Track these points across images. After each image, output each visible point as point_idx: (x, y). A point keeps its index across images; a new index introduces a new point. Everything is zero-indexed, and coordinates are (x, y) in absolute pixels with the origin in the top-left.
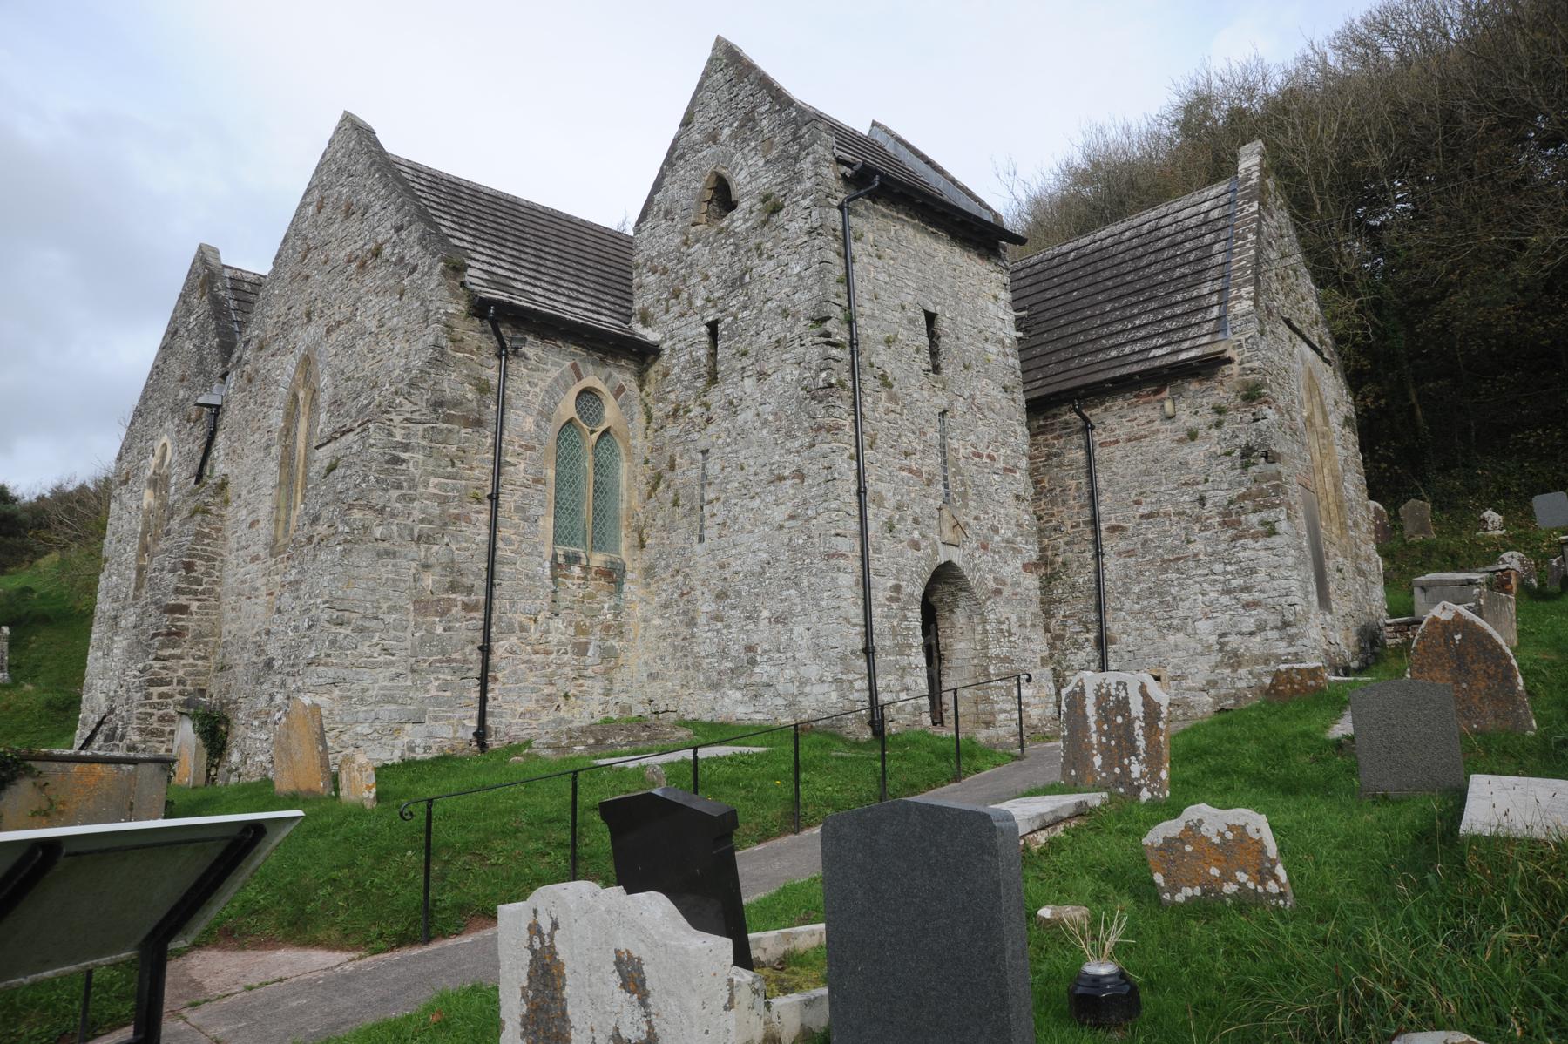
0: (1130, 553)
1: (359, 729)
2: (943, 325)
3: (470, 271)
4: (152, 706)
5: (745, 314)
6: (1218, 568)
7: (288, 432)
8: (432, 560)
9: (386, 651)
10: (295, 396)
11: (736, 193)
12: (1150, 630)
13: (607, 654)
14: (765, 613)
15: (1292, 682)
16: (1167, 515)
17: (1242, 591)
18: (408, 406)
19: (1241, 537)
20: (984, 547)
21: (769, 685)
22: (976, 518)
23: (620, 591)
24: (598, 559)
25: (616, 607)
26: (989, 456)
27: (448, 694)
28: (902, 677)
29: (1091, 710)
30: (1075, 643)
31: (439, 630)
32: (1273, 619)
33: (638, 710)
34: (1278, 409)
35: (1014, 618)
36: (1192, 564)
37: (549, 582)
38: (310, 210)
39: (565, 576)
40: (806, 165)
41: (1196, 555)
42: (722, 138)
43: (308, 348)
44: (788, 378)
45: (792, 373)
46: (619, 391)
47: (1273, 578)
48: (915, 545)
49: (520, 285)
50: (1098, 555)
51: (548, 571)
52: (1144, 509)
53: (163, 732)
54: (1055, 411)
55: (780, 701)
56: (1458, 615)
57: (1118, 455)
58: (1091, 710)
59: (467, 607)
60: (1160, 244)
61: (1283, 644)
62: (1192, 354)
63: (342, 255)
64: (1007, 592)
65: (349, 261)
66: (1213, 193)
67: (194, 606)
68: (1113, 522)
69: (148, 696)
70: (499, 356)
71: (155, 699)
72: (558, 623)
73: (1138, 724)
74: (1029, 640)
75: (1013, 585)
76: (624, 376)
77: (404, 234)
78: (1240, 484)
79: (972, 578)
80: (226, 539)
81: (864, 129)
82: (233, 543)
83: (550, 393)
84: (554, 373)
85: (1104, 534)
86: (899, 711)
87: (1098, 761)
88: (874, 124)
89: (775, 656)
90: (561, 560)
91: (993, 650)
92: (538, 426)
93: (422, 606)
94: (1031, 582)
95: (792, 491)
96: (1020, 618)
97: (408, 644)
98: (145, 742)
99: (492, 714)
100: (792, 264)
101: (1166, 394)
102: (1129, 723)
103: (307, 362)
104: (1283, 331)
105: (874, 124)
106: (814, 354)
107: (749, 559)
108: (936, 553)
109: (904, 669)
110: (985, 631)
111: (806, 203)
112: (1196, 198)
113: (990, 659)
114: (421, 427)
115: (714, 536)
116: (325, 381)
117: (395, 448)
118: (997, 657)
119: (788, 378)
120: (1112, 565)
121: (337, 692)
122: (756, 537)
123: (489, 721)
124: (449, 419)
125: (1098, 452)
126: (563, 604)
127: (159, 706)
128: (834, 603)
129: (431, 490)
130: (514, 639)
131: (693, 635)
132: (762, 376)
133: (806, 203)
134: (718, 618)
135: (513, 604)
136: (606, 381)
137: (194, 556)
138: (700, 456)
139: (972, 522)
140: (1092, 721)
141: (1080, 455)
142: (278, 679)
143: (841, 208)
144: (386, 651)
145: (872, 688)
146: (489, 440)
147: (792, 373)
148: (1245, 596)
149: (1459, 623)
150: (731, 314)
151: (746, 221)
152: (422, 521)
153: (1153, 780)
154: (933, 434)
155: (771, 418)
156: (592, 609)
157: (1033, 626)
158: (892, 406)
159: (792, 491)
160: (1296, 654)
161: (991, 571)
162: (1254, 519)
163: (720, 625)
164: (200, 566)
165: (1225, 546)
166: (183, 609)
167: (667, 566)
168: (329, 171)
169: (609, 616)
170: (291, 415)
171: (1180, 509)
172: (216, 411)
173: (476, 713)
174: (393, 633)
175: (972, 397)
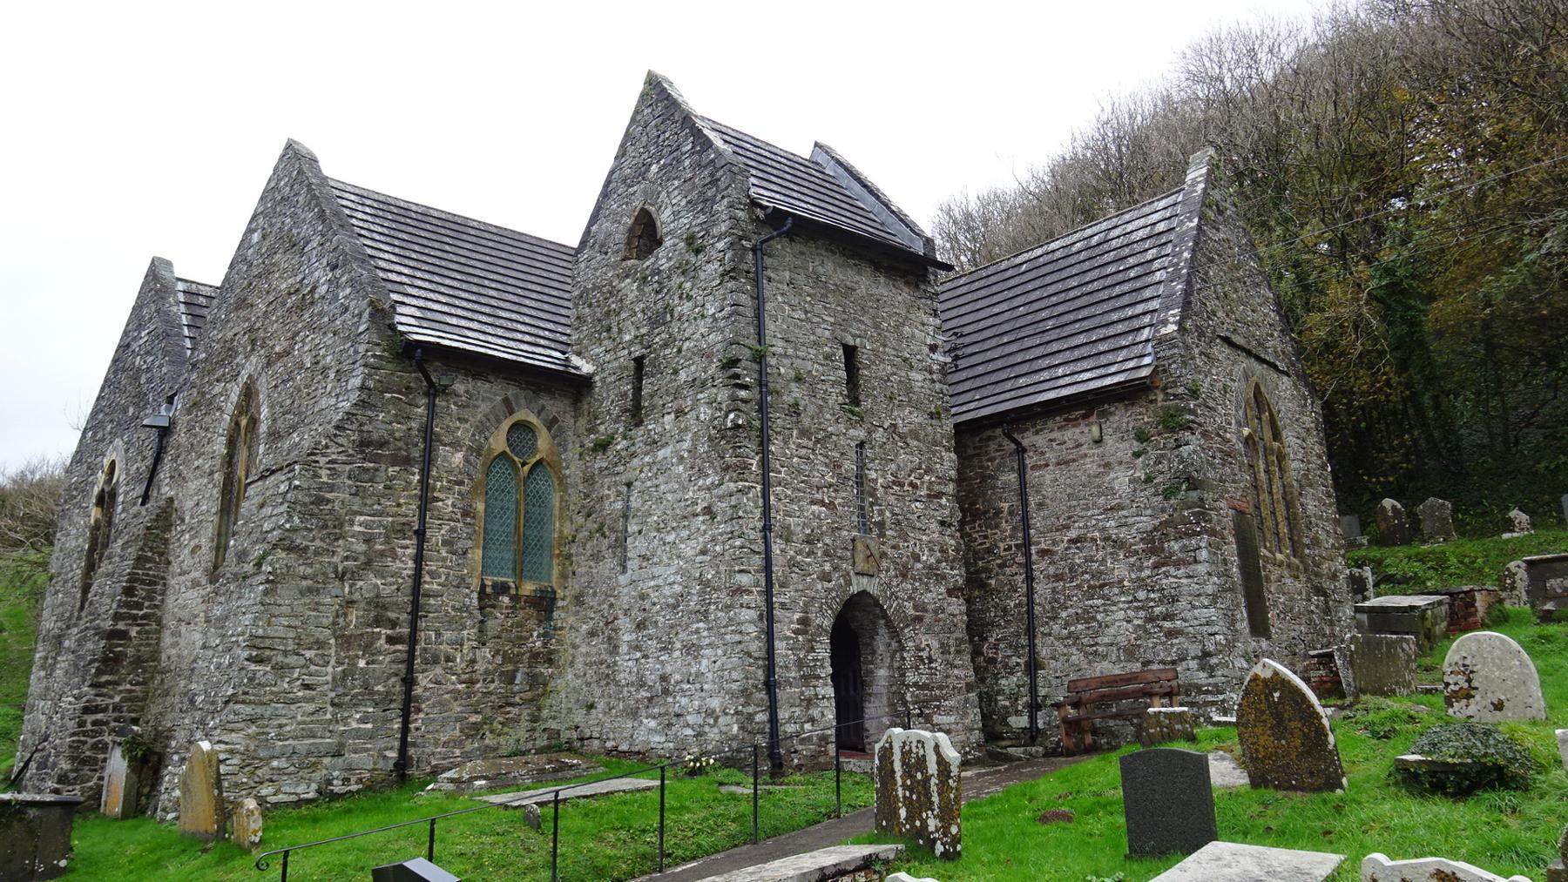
0: (1058, 577)
1: (275, 763)
2: (863, 358)
3: (400, 309)
4: (84, 733)
5: (667, 351)
6: (1141, 595)
8: (357, 596)
9: (306, 687)
10: (237, 424)
11: (662, 230)
13: (534, 680)
14: (678, 645)
15: (1159, 724)
16: (1094, 540)
19: (1163, 565)
20: (904, 576)
21: (678, 715)
22: (893, 547)
23: (550, 618)
24: (528, 588)
25: (545, 635)
26: (911, 484)
27: (369, 726)
28: (808, 708)
29: (897, 766)
30: (1006, 666)
31: (362, 663)
32: (1194, 649)
33: (565, 736)
34: (1205, 434)
35: (935, 644)
36: (1116, 590)
37: (477, 613)
38: (256, 237)
39: (494, 607)
40: (720, 207)
41: (1121, 581)
42: (650, 175)
43: (250, 377)
45: (705, 412)
46: (551, 423)
47: (1194, 607)
48: (825, 577)
49: (454, 321)
50: (1030, 579)
51: (475, 602)
52: (1073, 534)
53: (96, 759)
54: (989, 433)
55: (689, 732)
56: (1276, 673)
58: (897, 766)
59: (391, 640)
60: (1106, 258)
61: (1202, 675)
62: (1116, 379)
63: (284, 286)
64: (928, 617)
65: (290, 294)
66: (1162, 204)
67: (133, 632)
68: (1043, 546)
69: (81, 724)
70: (427, 394)
71: (89, 727)
72: (486, 652)
73: (934, 781)
74: (954, 666)
75: (936, 612)
76: (556, 406)
77: (338, 272)
78: (1163, 511)
79: (891, 607)
80: (169, 563)
81: (805, 151)
82: (175, 568)
83: (482, 428)
84: (484, 408)
85: (1034, 557)
86: (803, 741)
87: (903, 813)
88: (816, 145)
89: (686, 686)
90: (489, 590)
91: (911, 677)
93: (345, 641)
94: (956, 606)
96: (942, 645)
97: (329, 678)
98: (76, 771)
99: (414, 744)
100: (708, 305)
101: (1093, 418)
102: (927, 779)
103: (249, 393)
104: (1221, 351)
105: (816, 145)
106: (723, 395)
107: (667, 591)
108: (849, 583)
109: (809, 700)
110: (903, 659)
112: (1147, 210)
113: (908, 686)
114: (348, 468)
115: (636, 567)
116: (265, 412)
117: (320, 489)
118: (915, 684)
119: (702, 417)
120: (1042, 589)
121: (253, 729)
122: (672, 570)
123: (411, 751)
124: (375, 459)
125: (1032, 476)
126: (490, 634)
127: (94, 734)
128: (737, 638)
129: (357, 528)
130: (439, 670)
131: (615, 663)
132: (680, 413)
133: (720, 245)
134: (637, 648)
135: (438, 634)
136: (539, 413)
137: (136, 580)
138: (625, 489)
139: (889, 551)
140: (898, 775)
141: (1012, 477)
142: (198, 715)
143: (754, 250)
144: (306, 687)
145: (773, 720)
146: (417, 477)
147: (705, 412)
148: (1167, 624)
149: (1278, 681)
151: (669, 259)
152: (346, 558)
153: (945, 835)
154: (849, 466)
156: (521, 638)
157: (958, 652)
158: (804, 442)
160: (1216, 685)
161: (910, 598)
162: (1175, 546)
163: (639, 655)
164: (141, 591)
165: (1147, 572)
166: (123, 635)
167: (595, 594)
168: (274, 201)
169: (538, 644)
170: (232, 443)
172: (165, 432)
173: (397, 744)
174: (313, 668)
175: (894, 426)
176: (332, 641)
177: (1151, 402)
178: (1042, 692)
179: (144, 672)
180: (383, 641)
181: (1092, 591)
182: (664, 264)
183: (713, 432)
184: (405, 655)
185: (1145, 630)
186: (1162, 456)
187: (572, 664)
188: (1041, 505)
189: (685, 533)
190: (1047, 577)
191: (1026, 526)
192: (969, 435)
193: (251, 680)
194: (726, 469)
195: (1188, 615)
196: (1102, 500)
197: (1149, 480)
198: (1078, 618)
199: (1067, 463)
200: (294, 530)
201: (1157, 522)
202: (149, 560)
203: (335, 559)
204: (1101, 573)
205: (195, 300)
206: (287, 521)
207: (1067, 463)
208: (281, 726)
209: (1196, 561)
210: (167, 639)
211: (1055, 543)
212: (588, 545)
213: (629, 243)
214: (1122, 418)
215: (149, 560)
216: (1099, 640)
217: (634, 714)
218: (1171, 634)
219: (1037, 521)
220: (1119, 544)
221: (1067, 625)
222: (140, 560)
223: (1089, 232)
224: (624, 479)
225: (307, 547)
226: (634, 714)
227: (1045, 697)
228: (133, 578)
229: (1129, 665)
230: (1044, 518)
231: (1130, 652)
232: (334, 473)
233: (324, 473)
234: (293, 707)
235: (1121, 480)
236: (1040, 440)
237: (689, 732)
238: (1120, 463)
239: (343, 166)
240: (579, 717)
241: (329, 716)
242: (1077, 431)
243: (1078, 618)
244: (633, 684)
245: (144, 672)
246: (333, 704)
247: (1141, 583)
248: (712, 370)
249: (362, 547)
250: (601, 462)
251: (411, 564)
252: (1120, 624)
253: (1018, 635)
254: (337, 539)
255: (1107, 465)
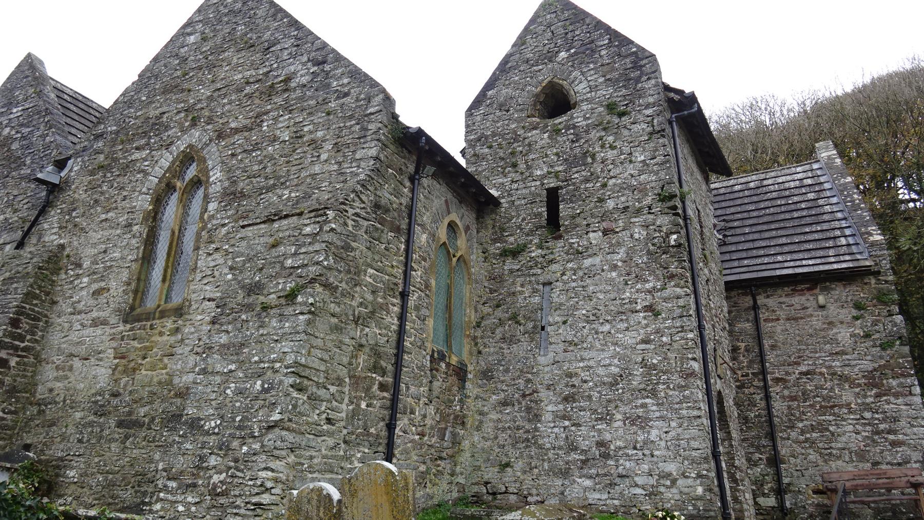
6: (868, 415)
7: (154, 217)
12: (813, 456)
14: (619, 416)
16: (821, 374)
17: (888, 433)
18: (357, 204)
19: (885, 395)
31: (363, 405)
36: (846, 411)
41: (849, 404)
42: (559, 59)
44: (636, 236)
47: (913, 426)
50: (767, 397)
52: (804, 368)
55: (639, 491)
57: (779, 329)
67: (13, 363)
68: (777, 375)
78: (881, 357)
85: (770, 383)
89: (630, 452)
90: (436, 355)
92: (428, 242)
93: (356, 380)
95: (644, 322)
97: (343, 415)
111: (649, 112)
114: (366, 223)
119: (636, 236)
120: (779, 406)
121: (292, 459)
125: (766, 327)
131: (536, 429)
133: (649, 112)
137: (22, 314)
141: (748, 326)
148: (891, 437)
150: (574, 184)
151: (586, 119)
155: (620, 264)
159: (644, 322)
162: (894, 383)
163: (567, 423)
164: (25, 324)
171: (832, 371)
176: (347, 380)
177: (866, 284)
178: (786, 480)
179: (17, 401)
180: (376, 387)
181: (824, 410)
182: (580, 122)
183: (652, 248)
184: (388, 403)
185: (873, 441)
186: (877, 321)
187: (478, 429)
188: (773, 347)
189: (623, 326)
190: (783, 397)
191: (762, 362)
192: (745, 290)
193: (295, 407)
194: (672, 277)
195: (909, 431)
196: (828, 347)
197: (867, 336)
198: (813, 428)
199: (796, 319)
200: (329, 268)
201: (876, 365)
202: (36, 297)
203: (354, 303)
204: (831, 397)
205: (61, 95)
206: (325, 259)
207: (796, 319)
208: (311, 458)
209: (911, 394)
210: (49, 372)
211: (787, 373)
212: (498, 331)
213: (535, 105)
214: (840, 292)
215: (36, 297)
216: (833, 445)
217: (565, 473)
218: (894, 444)
219: (771, 357)
220: (844, 378)
221: (803, 432)
222: (29, 296)
223: (749, 179)
224: (542, 279)
225: (337, 287)
226: (565, 473)
227: (789, 484)
228: (20, 311)
229: (861, 465)
230: (777, 356)
231: (861, 455)
232: (357, 226)
233: (350, 223)
234: (319, 439)
235: (844, 335)
236: (771, 302)
237: (639, 491)
238: (842, 323)
239: (55, 70)
240: (491, 474)
241: (342, 453)
242: (804, 298)
243: (813, 428)
244: (560, 448)
245: (17, 401)
246: (345, 442)
247: (867, 407)
248: (648, 200)
249: (369, 297)
250: (510, 264)
251: (396, 321)
252: (850, 434)
253: (759, 438)
254: (356, 285)
255: (831, 323)
